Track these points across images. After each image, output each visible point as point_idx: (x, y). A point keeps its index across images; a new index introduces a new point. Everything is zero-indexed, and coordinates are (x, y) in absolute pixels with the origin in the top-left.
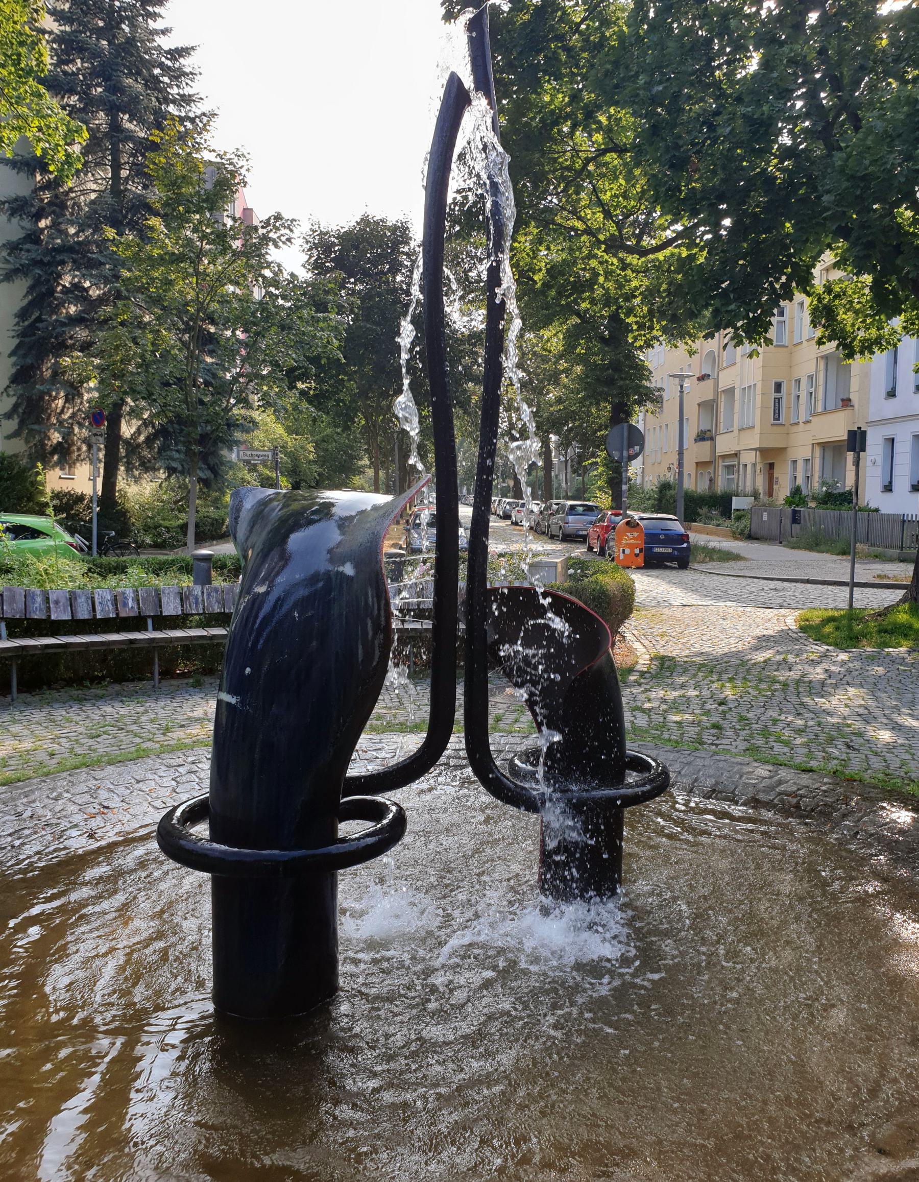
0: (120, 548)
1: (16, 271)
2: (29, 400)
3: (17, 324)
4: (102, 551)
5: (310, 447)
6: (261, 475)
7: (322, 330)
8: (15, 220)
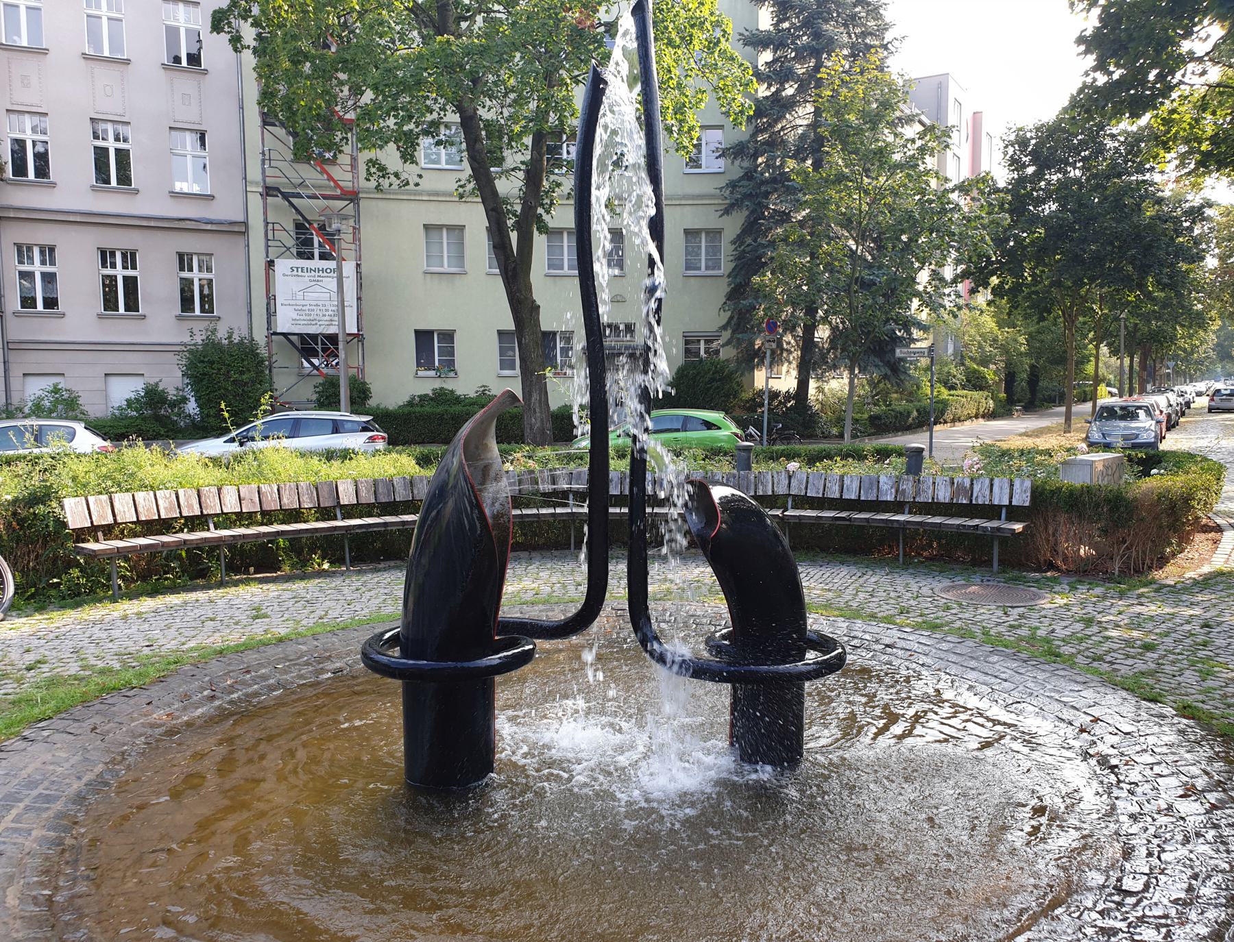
0: (786, 439)
1: (732, 206)
2: (740, 313)
3: (735, 249)
4: (772, 442)
5: (1022, 339)
6: (968, 368)
7: (976, 228)
8: (737, 163)
